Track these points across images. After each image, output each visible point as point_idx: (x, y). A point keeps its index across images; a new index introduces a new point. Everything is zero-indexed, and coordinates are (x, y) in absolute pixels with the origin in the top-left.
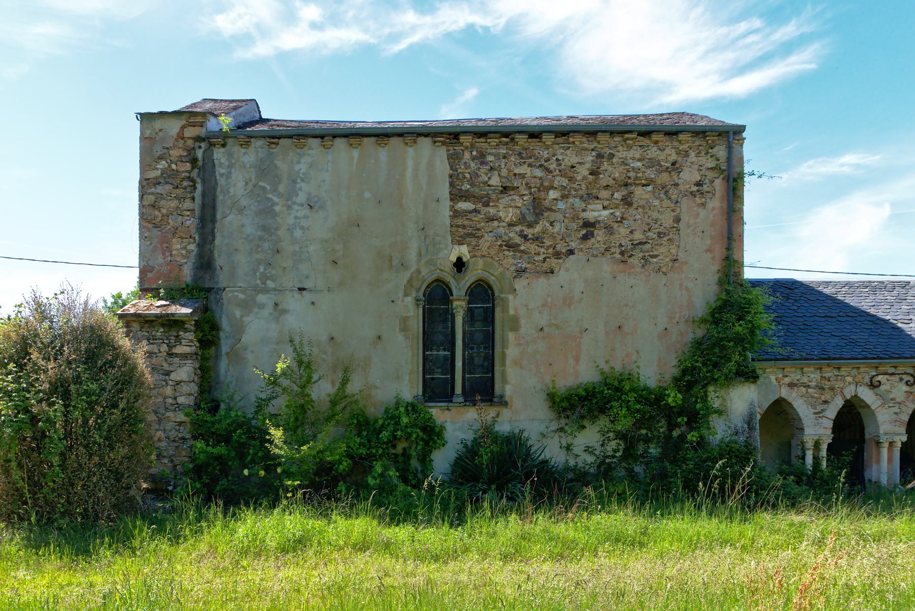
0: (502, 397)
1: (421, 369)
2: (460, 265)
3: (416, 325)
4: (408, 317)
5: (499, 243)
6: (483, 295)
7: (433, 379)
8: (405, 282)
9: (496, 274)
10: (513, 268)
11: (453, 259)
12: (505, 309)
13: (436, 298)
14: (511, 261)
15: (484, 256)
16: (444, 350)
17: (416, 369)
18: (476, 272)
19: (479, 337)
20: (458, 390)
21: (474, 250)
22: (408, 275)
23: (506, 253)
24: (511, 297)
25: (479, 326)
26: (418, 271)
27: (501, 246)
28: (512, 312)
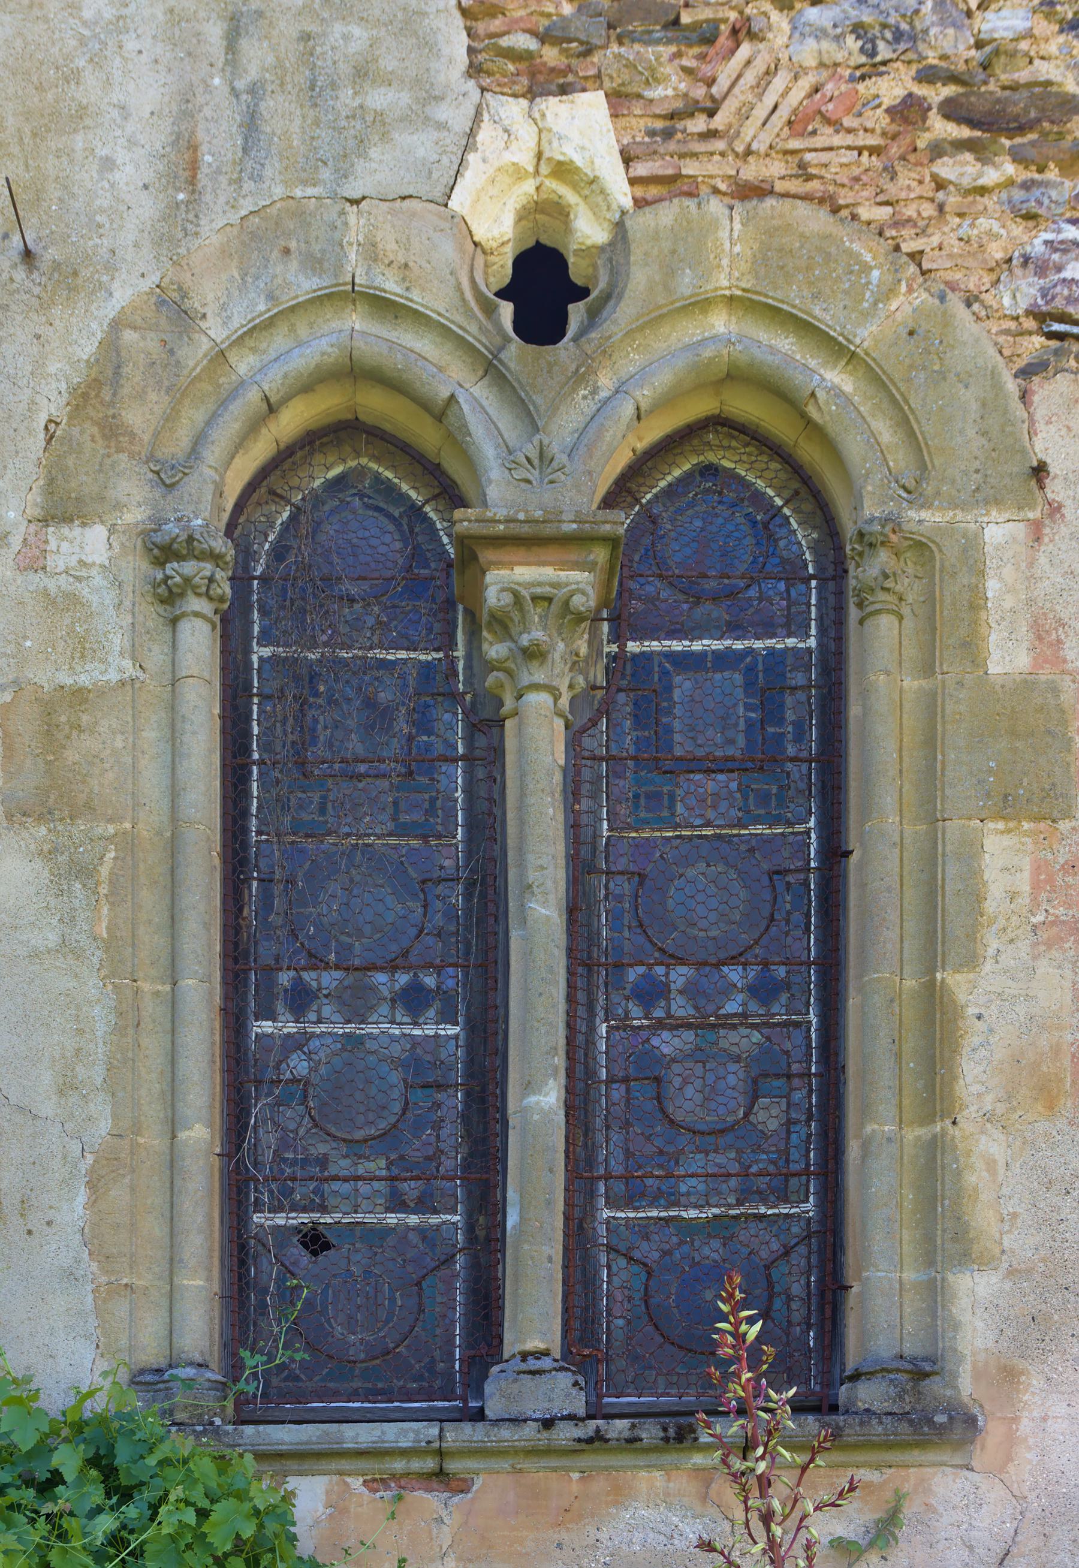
0: (921, 1370)
1: (201, 1134)
2: (543, 290)
3: (163, 762)
4: (79, 696)
5: (891, 88)
6: (757, 552)
7: (315, 1241)
8: (52, 402)
9: (865, 336)
10: (1021, 293)
11: (496, 224)
12: (950, 631)
13: (333, 578)
14: (997, 232)
15: (750, 192)
16: (413, 1000)
17: (153, 1140)
18: (687, 331)
19: (708, 901)
20: (534, 1319)
21: (666, 146)
22: (77, 338)
23: (959, 169)
24: (999, 531)
25: (706, 807)
26: (175, 310)
27: (909, 112)
28: (1006, 656)
